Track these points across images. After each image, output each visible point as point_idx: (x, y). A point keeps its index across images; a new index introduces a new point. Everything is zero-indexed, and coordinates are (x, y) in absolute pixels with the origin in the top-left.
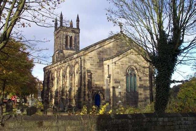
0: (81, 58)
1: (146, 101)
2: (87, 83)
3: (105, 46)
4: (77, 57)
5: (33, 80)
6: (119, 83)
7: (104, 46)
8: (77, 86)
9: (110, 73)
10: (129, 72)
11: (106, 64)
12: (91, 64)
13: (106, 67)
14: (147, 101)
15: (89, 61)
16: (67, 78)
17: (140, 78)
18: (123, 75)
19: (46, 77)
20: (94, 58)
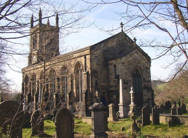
0: (85, 58)
1: (148, 102)
2: (95, 84)
5: (97, 91)
6: (127, 84)
9: (117, 74)
11: (111, 64)
12: (97, 64)
13: (111, 67)
17: (144, 79)
18: (130, 76)
19: (110, 45)
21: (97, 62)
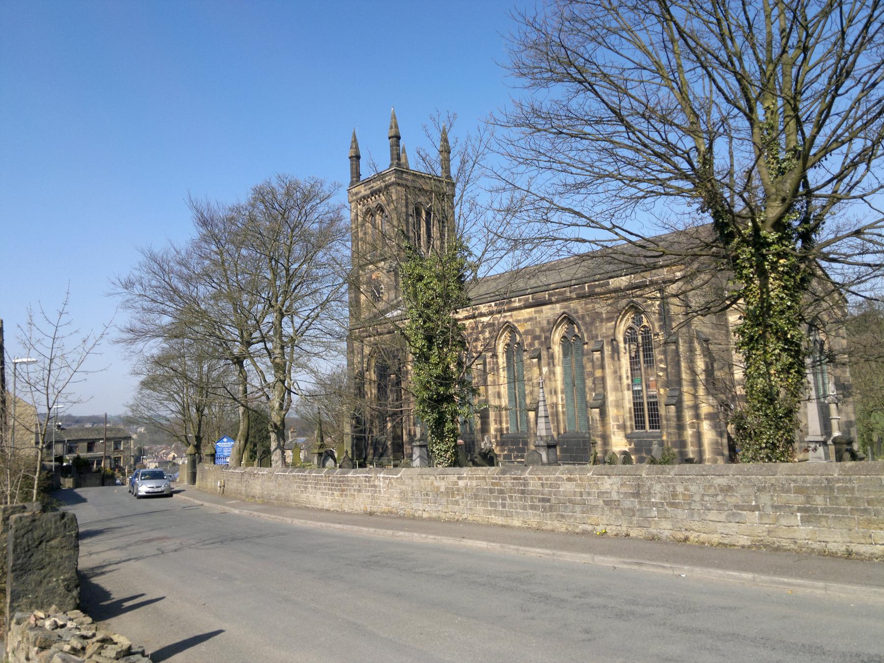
8: (628, 389)
16: (556, 361)
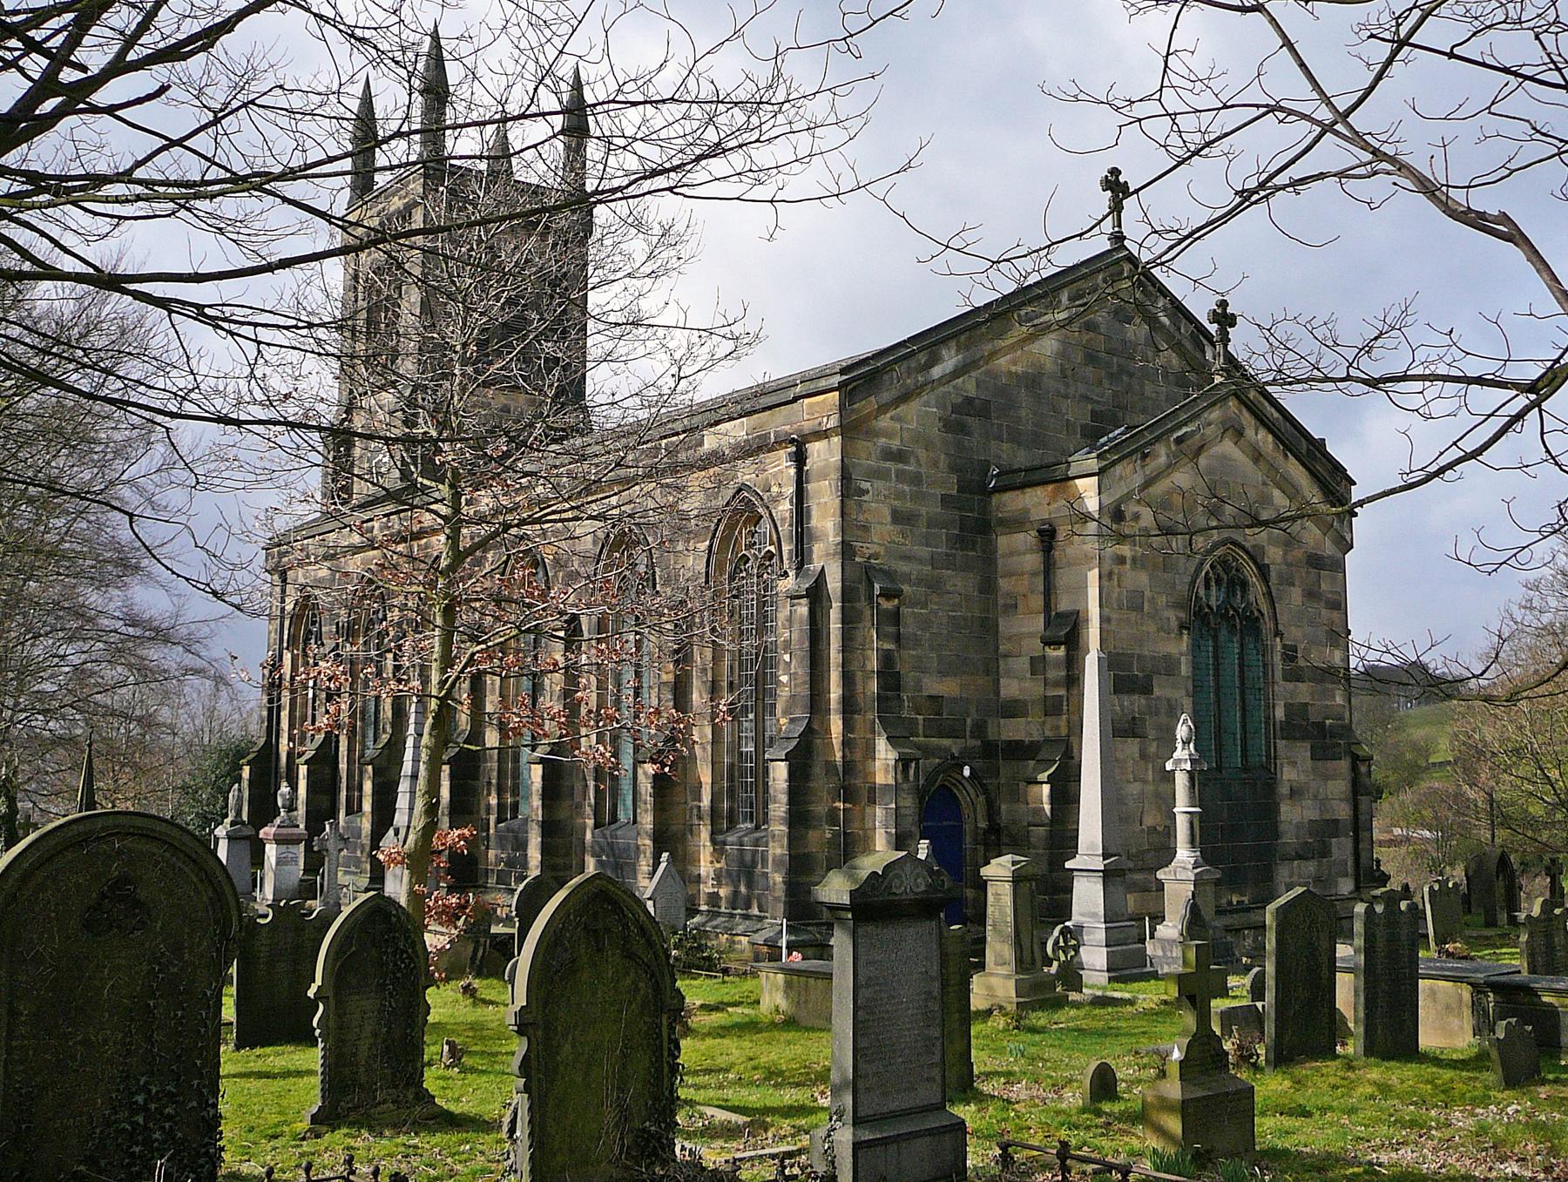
0: (800, 459)
1: (1324, 852)
2: (874, 686)
3: (1003, 362)
4: (755, 449)
6: (1147, 690)
7: (994, 354)
10: (1208, 596)
11: (1017, 523)
12: (898, 517)
14: (1334, 850)
15: (880, 484)
17: (1290, 654)
18: (1174, 624)
20: (918, 461)
21: (900, 495)
